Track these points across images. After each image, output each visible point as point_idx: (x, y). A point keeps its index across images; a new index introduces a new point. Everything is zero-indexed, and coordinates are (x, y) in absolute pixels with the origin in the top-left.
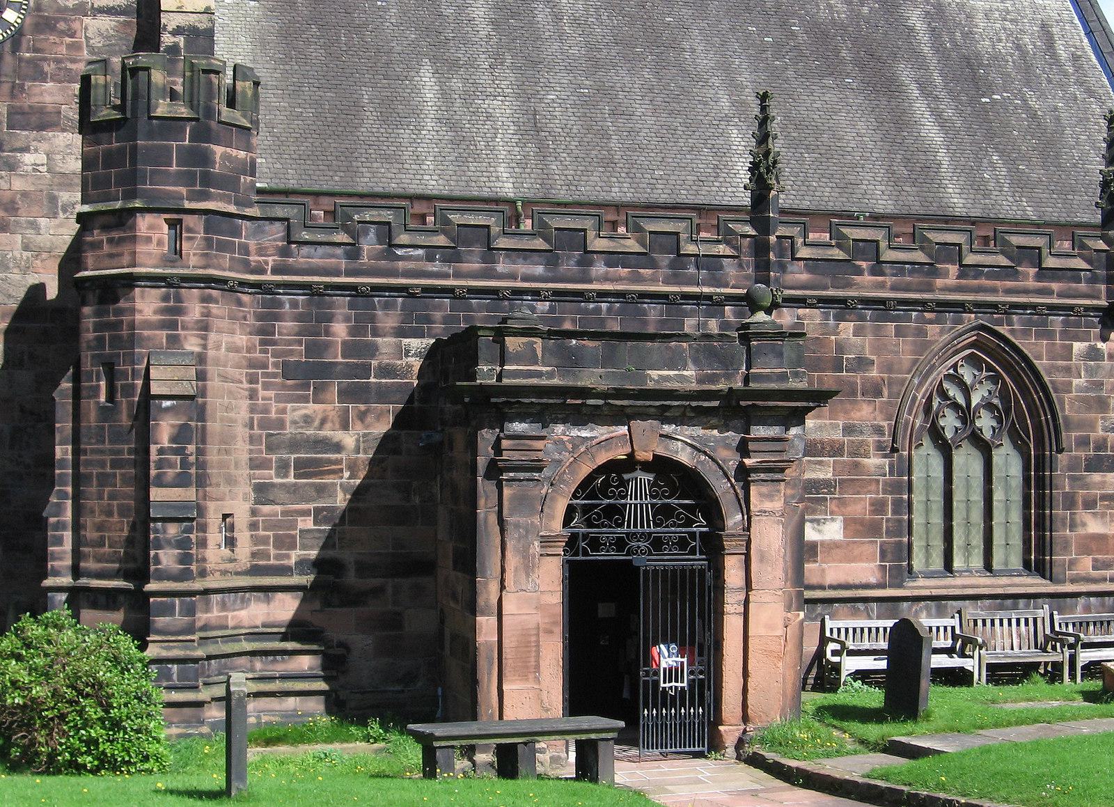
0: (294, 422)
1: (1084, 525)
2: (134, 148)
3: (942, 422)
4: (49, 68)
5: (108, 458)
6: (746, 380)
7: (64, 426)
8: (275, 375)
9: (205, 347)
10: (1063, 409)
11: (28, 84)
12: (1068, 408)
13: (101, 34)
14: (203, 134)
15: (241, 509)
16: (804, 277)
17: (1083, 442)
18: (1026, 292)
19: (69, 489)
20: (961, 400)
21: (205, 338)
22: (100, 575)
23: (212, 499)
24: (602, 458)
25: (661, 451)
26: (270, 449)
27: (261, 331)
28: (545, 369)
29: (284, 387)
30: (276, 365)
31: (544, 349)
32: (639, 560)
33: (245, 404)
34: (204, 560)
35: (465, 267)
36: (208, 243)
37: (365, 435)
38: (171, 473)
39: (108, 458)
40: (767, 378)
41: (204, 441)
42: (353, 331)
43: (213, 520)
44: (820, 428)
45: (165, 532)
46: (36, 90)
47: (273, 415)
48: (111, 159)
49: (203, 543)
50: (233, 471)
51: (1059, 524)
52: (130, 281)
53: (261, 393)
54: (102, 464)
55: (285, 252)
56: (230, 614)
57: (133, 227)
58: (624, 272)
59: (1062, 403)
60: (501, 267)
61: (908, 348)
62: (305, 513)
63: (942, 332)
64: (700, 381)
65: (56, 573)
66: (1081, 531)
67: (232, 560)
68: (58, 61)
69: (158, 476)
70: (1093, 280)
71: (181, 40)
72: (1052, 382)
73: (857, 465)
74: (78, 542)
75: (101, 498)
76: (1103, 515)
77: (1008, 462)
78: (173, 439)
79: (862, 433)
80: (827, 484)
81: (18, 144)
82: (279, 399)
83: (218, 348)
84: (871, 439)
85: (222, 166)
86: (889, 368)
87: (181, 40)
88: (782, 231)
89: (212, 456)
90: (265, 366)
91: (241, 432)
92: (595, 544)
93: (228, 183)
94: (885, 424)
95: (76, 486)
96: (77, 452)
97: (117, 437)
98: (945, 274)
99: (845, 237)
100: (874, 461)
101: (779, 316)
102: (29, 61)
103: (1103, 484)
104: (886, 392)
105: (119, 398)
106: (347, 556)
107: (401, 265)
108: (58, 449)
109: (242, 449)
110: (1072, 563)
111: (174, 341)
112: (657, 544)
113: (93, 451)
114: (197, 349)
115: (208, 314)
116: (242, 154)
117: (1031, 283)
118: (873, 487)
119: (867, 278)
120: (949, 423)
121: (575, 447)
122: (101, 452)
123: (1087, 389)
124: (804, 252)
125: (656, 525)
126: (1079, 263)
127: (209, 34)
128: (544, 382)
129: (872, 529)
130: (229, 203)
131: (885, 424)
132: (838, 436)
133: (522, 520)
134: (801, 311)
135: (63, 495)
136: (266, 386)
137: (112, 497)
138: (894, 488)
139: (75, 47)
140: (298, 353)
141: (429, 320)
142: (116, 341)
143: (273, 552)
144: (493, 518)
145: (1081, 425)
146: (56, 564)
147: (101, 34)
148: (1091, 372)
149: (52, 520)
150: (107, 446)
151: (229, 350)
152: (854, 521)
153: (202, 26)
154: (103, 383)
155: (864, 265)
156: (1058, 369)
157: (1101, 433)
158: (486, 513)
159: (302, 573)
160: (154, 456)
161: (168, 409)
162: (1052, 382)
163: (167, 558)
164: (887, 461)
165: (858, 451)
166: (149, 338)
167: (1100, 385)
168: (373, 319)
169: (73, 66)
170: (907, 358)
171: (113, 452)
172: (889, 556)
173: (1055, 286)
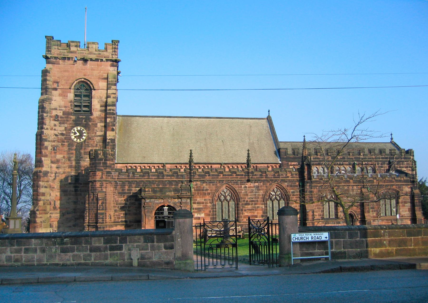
0: (120, 201)
1: (244, 214)
2: (96, 162)
3: (221, 198)
4: (90, 145)
5: (93, 206)
6: (181, 194)
7: (87, 202)
8: (117, 194)
9: (106, 190)
10: (240, 196)
11: (87, 148)
12: (241, 195)
13: (98, 140)
14: (106, 160)
15: (112, 213)
16: (198, 177)
17: (244, 201)
18: (234, 178)
19: (88, 211)
20: (224, 195)
21: (106, 189)
22: (92, 223)
23: (107, 212)
24: (160, 205)
25: (168, 204)
26: (116, 205)
27: (115, 188)
28: (151, 193)
29: (118, 196)
30: (117, 192)
31: (151, 190)
32: (166, 220)
33: (113, 198)
34: (106, 221)
35: (145, 177)
36: (107, 175)
37: (130, 202)
38: (101, 208)
39: (93, 206)
40: (184, 193)
41: (106, 204)
42: (129, 187)
43: (108, 215)
44: (200, 200)
45: (100, 216)
46: (88, 149)
47: (117, 200)
48: (93, 164)
49: (106, 218)
50: (111, 208)
51: (240, 214)
52: (95, 181)
53: (115, 197)
54: (92, 207)
55: (118, 176)
56: (110, 229)
57: (96, 173)
58: (169, 177)
59: (240, 195)
60: (151, 177)
61: (215, 187)
62: (122, 214)
63: (220, 185)
64: (174, 194)
65: (86, 223)
66: (244, 215)
67: (111, 221)
68: (91, 144)
69: (99, 209)
70: (245, 176)
71: (110, 141)
72: (238, 192)
73: (206, 205)
74: (89, 218)
75: (92, 212)
76: (248, 212)
77: (232, 203)
78: (101, 204)
79: (207, 200)
80: (202, 208)
81: (85, 157)
82: (118, 197)
83: (108, 190)
84: (209, 201)
85: (109, 164)
86: (211, 190)
87: (110, 141)
88: (194, 170)
89: (107, 206)
90: (116, 193)
91: (112, 202)
92: (159, 217)
93: (110, 167)
94: (211, 199)
95: (89, 211)
96: (89, 205)
97: (94, 203)
98: (220, 176)
99: (204, 171)
100: (209, 205)
101: (194, 183)
102: (87, 144)
103: (247, 207)
104: (211, 194)
105: (94, 198)
106: (128, 220)
107: (136, 177)
108: (86, 205)
109: (112, 205)
110: (242, 220)
111: (102, 189)
112: (169, 217)
113: (91, 205)
114: (105, 191)
115: (107, 186)
116: (112, 162)
117: (235, 176)
118: (209, 208)
119: (208, 177)
120: (222, 198)
121: (156, 204)
122: (92, 205)
123: (244, 193)
124: (198, 173)
125: (169, 215)
126: (243, 173)
127: (114, 140)
128: (151, 195)
129: (209, 215)
130: (110, 169)
131: (211, 199)
132: (203, 201)
133: (148, 214)
134: (197, 182)
135: (87, 212)
136: (116, 196)
137: (93, 212)
138: (213, 208)
139: (94, 142)
140: (121, 191)
141: (140, 185)
142: (94, 190)
143: (117, 220)
144: (144, 214)
145: (244, 198)
146: (86, 222)
147: (98, 140)
148: (245, 190)
149: (85, 215)
150: (93, 205)
151: (110, 190)
152: (206, 214)
153: (113, 138)
154: (92, 196)
155: (207, 175)
156: (239, 190)
157: (247, 199)
158: (143, 213)
159: (121, 222)
160: (98, 206)
161: (100, 199)
162: (238, 192)
163: (100, 220)
164: (211, 205)
165: (206, 203)
166: (98, 189)
167: (247, 192)
168: (131, 185)
169: (94, 145)
170: (214, 189)
171: (94, 205)
172: (212, 219)
173: (239, 177)
